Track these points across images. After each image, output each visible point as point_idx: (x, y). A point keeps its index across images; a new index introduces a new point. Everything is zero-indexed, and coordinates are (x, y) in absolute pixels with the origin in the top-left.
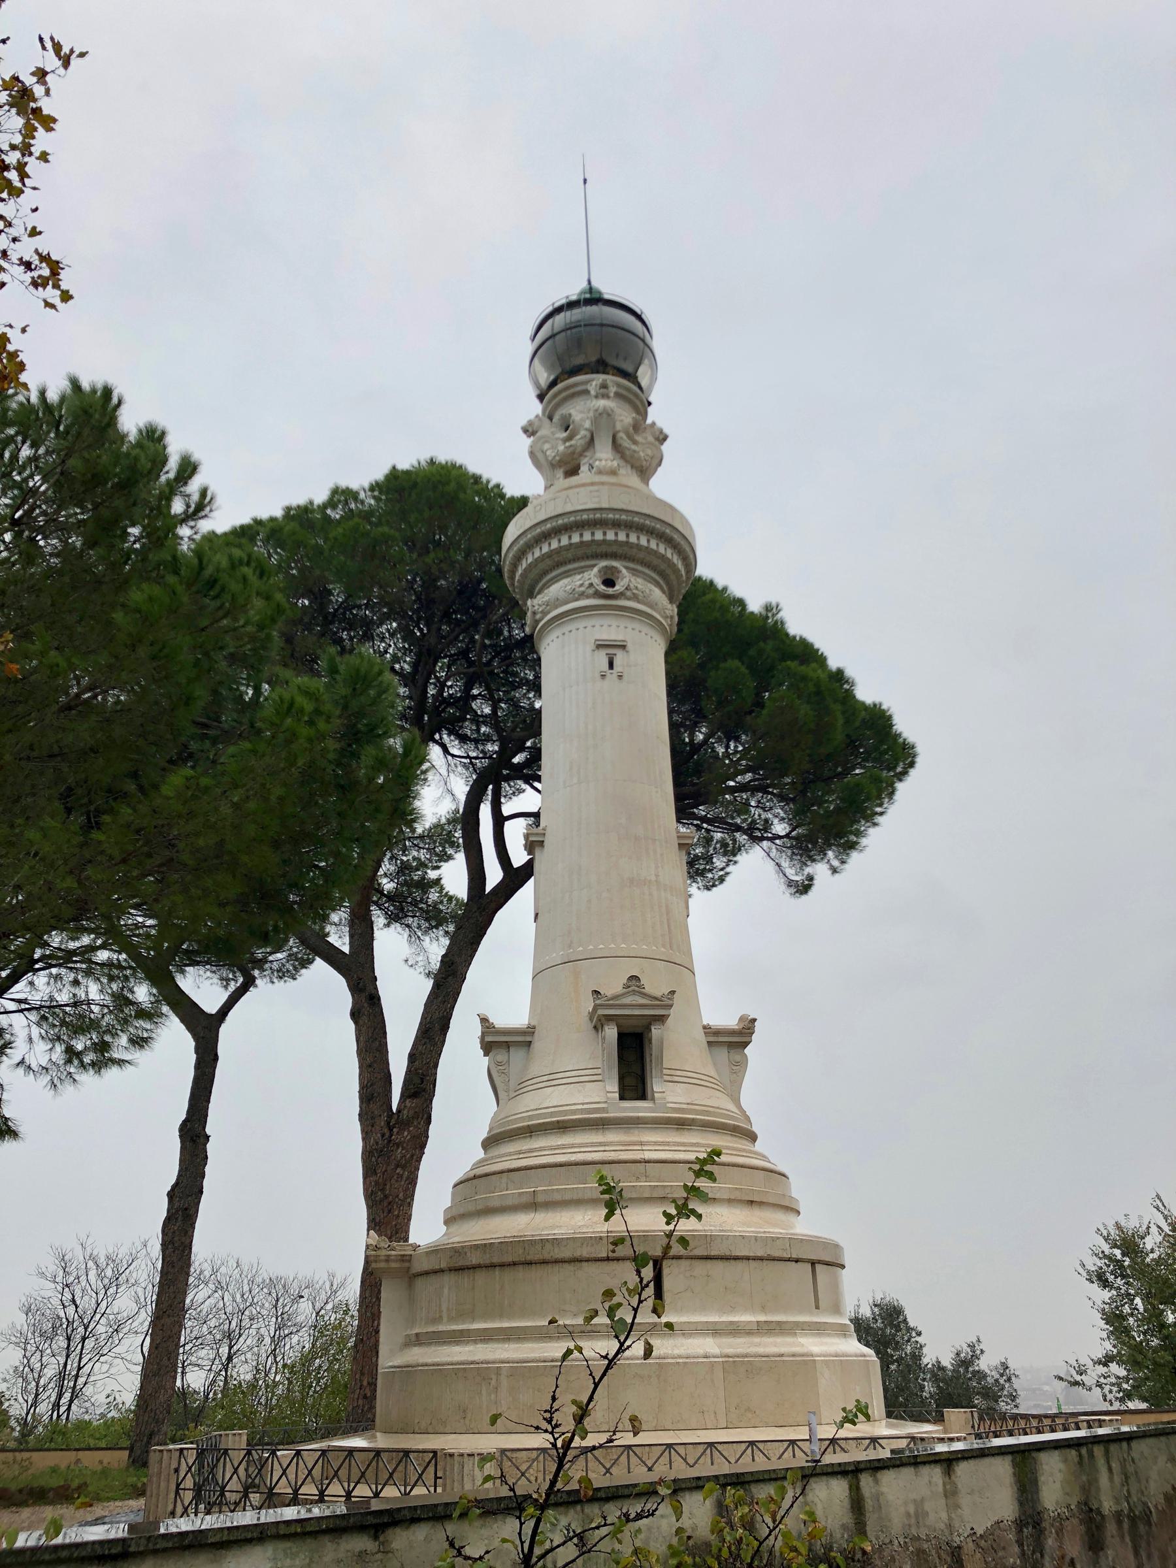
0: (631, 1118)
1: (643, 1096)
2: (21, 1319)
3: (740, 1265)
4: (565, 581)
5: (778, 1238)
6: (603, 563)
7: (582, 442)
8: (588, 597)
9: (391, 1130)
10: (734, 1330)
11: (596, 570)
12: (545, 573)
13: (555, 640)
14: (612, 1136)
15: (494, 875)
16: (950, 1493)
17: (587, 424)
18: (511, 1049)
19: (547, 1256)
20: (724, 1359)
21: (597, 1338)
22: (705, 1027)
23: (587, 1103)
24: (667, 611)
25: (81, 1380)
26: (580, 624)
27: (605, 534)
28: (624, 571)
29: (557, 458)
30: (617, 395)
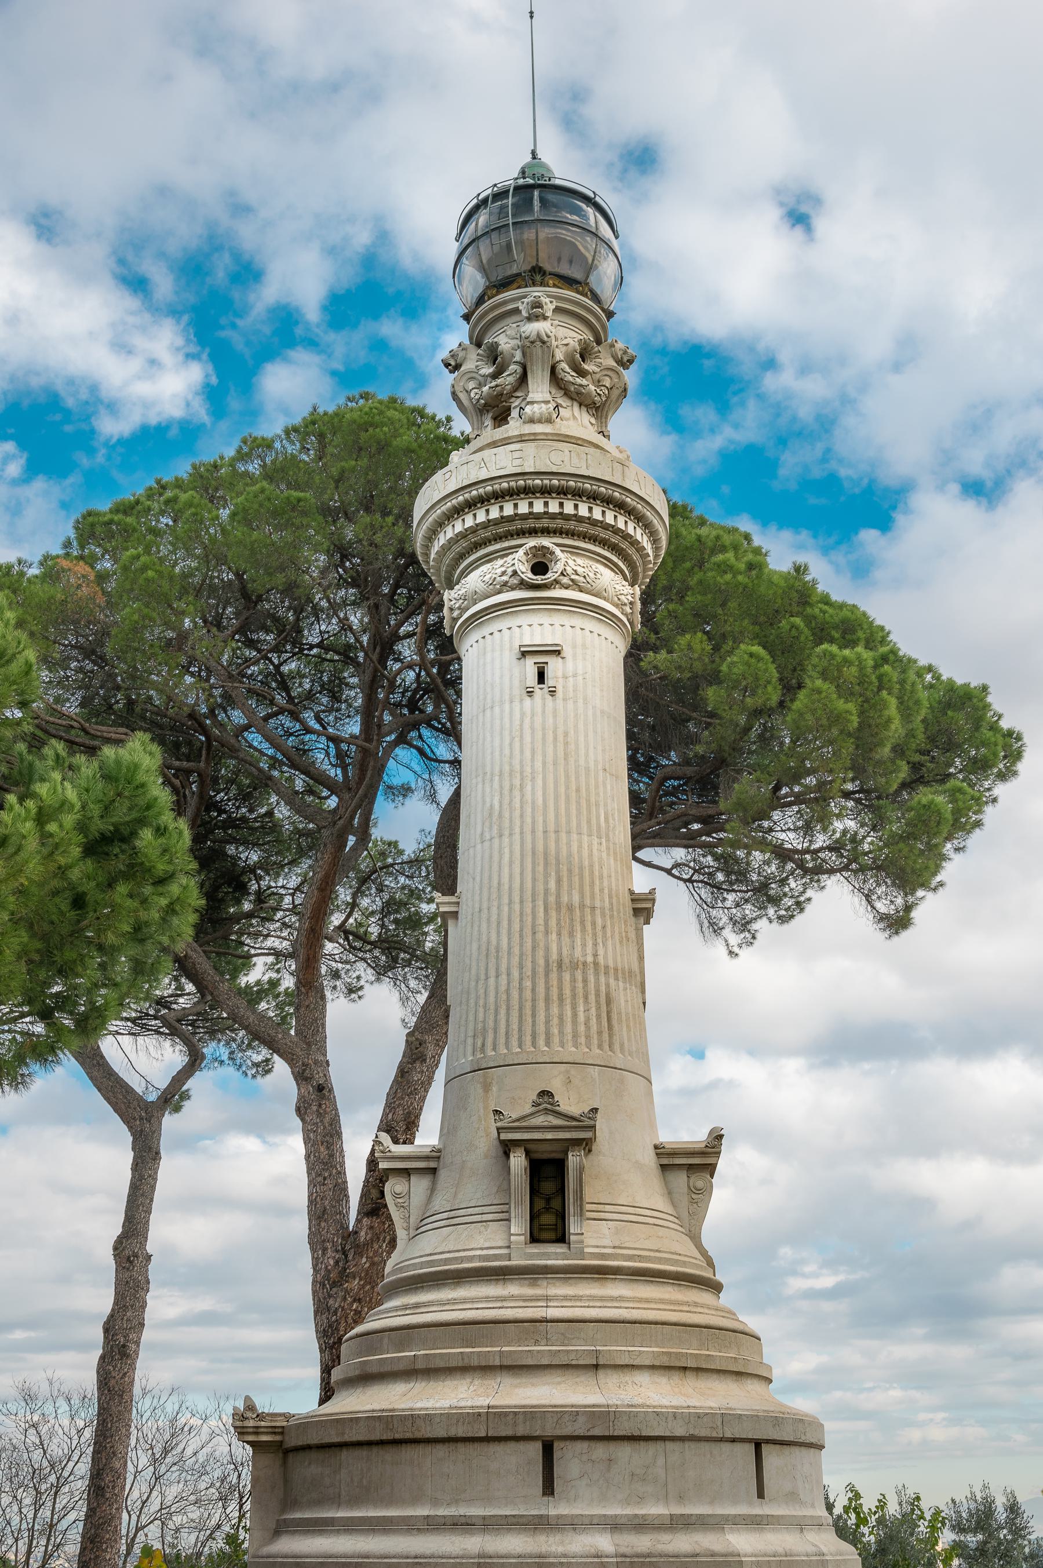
0: (538, 1266)
1: (561, 1238)
3: (652, 1448)
4: (484, 568)
5: (707, 1414)
6: (532, 542)
7: (511, 379)
8: (513, 589)
10: (641, 1525)
11: (521, 551)
12: (462, 556)
13: (475, 645)
14: (513, 1289)
17: (518, 356)
18: (412, 1178)
19: (418, 1435)
20: (619, 1560)
21: (472, 1533)
22: (656, 1147)
23: (487, 1248)
24: (622, 597)
26: (503, 624)
27: (531, 504)
28: (557, 551)
29: (483, 401)
30: (558, 310)
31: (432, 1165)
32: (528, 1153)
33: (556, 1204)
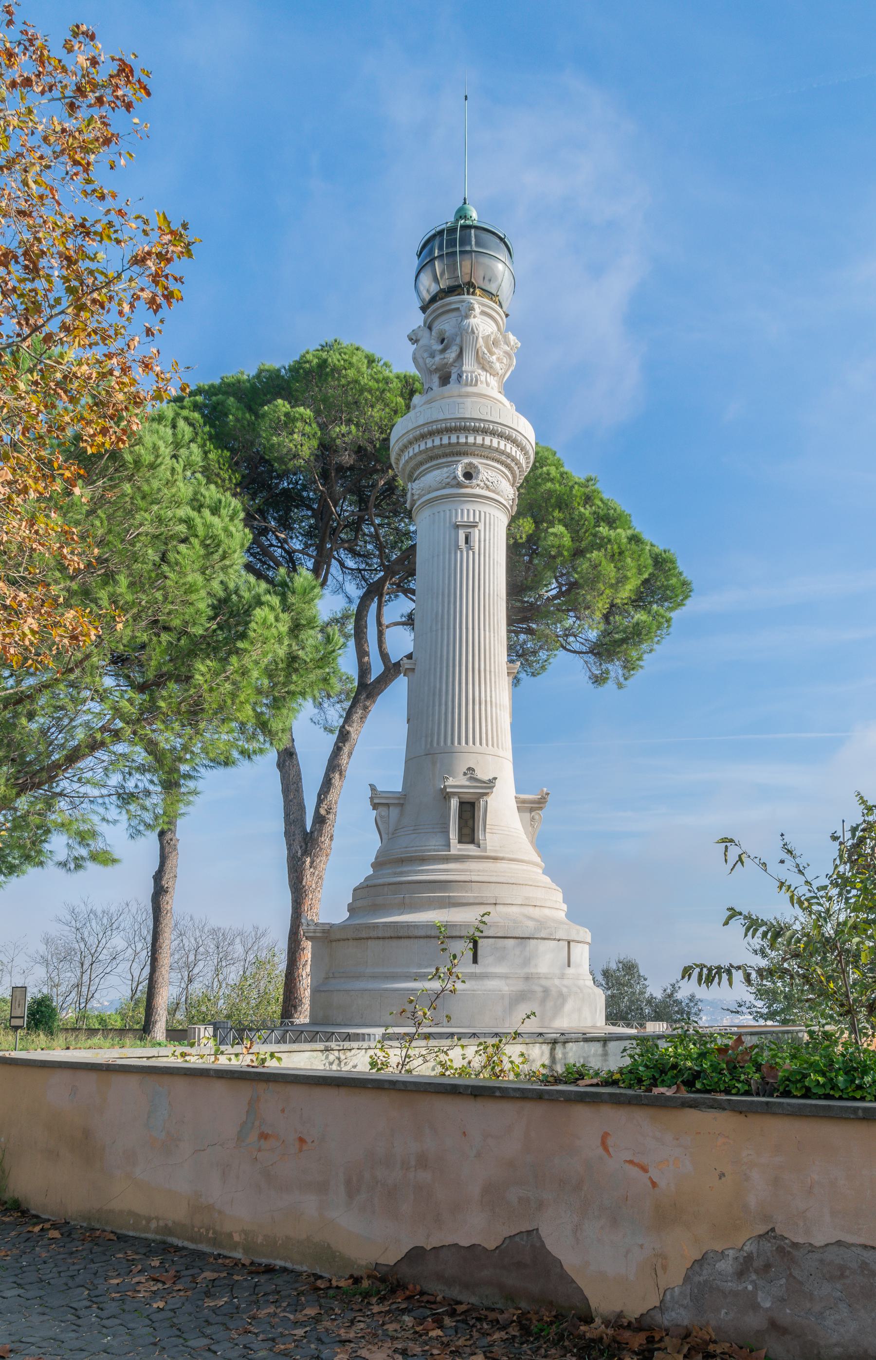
1: (472, 840)
2: (42, 949)
8: (452, 487)
9: (306, 844)
12: (421, 464)
15: (377, 668)
16: (605, 1054)
19: (411, 934)
25: (93, 988)
31: (402, 802)
32: (459, 798)
33: (470, 823)
